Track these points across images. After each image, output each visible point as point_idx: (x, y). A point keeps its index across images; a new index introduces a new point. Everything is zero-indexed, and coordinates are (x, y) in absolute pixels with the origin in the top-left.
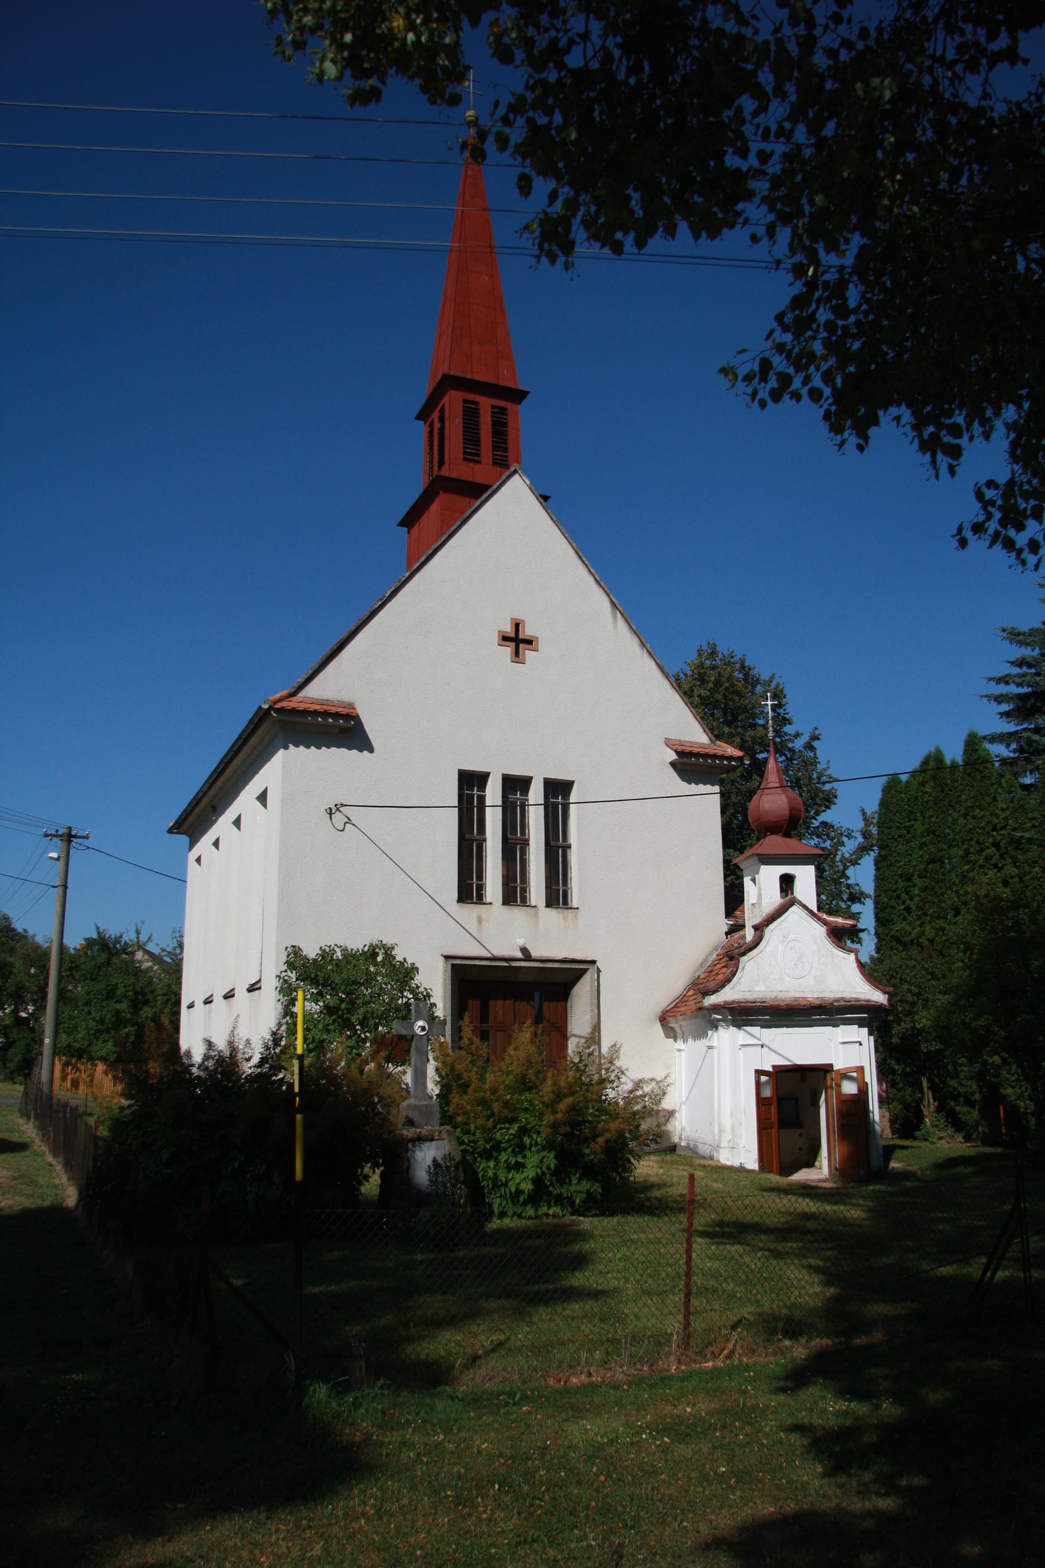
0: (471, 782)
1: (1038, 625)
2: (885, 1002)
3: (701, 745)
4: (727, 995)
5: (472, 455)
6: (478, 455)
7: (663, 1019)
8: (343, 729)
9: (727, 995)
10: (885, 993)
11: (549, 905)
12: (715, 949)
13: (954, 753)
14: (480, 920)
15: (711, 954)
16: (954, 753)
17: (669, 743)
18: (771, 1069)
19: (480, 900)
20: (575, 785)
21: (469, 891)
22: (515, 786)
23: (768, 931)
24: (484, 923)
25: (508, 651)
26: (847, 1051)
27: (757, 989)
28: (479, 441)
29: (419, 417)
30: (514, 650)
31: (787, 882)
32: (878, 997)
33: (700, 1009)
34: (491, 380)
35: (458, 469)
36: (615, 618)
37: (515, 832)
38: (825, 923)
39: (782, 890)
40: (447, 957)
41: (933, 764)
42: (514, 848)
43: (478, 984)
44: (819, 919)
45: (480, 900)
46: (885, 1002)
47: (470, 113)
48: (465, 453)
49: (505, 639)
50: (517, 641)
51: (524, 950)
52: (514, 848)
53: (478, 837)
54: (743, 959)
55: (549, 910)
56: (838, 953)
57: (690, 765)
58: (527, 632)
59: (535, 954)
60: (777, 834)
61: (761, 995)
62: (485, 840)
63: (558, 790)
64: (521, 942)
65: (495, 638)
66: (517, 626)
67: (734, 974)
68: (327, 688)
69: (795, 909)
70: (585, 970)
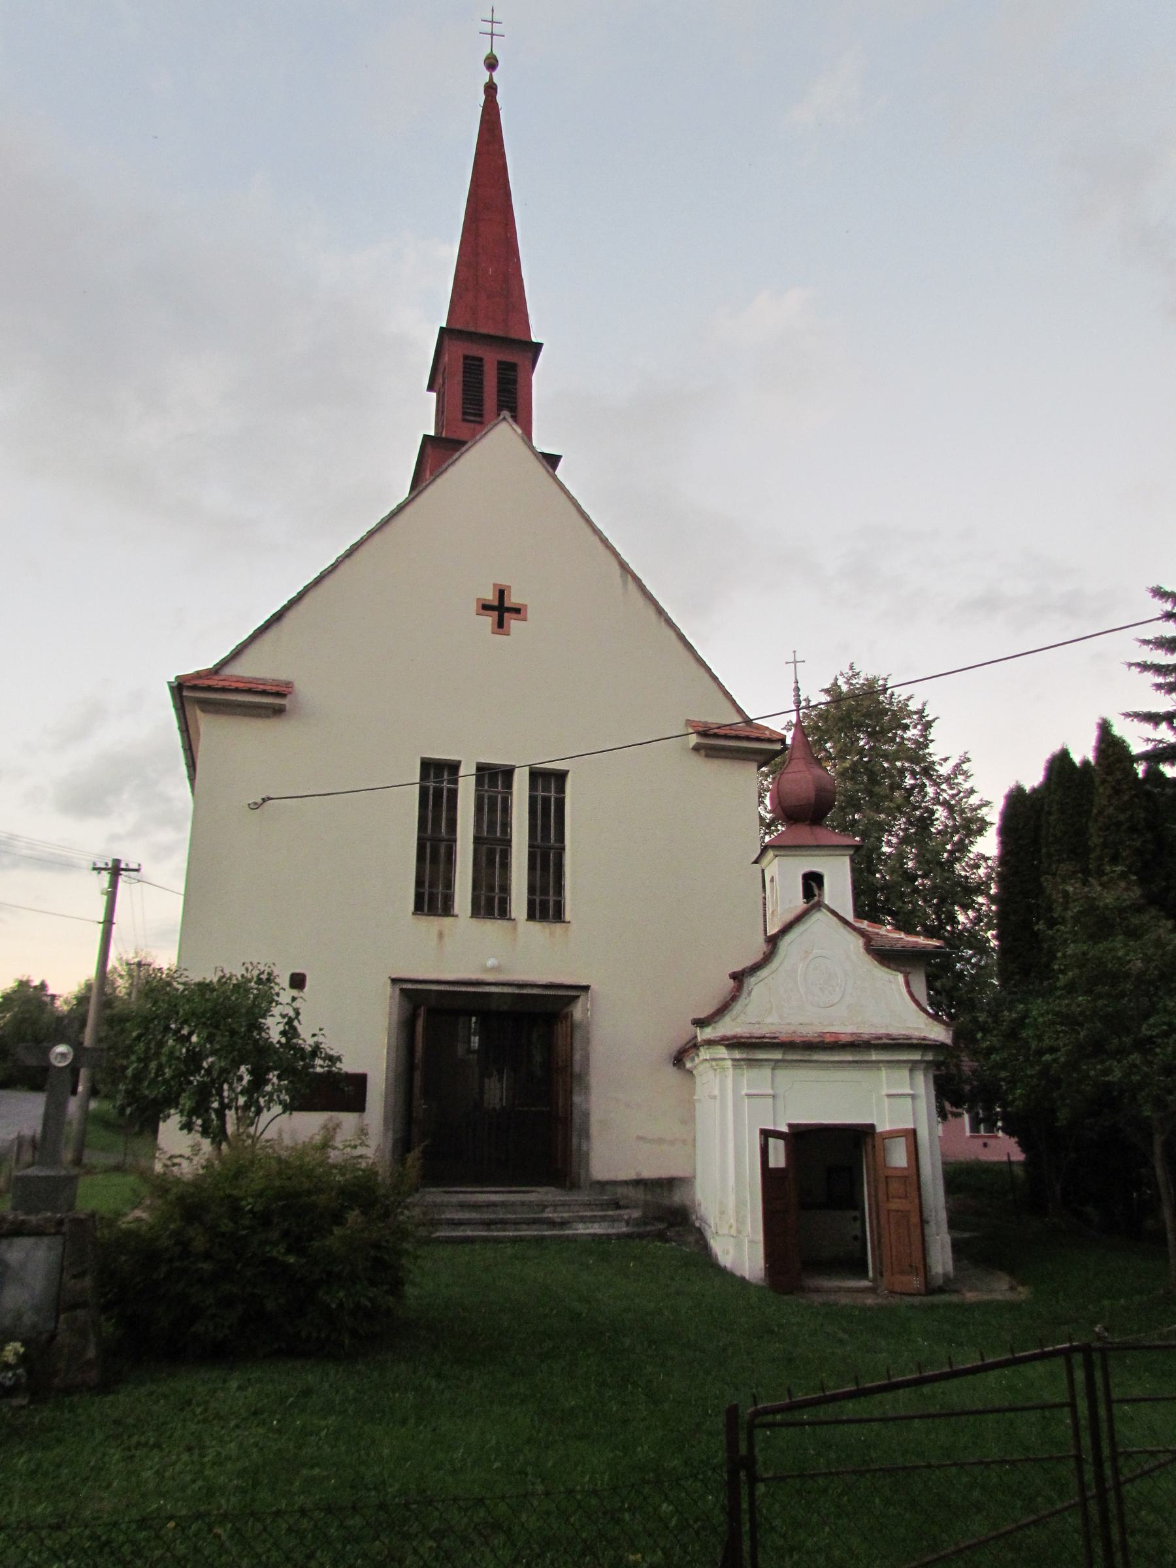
0: (437, 775)
1: (1171, 709)
2: (948, 1041)
6: (481, 415)
9: (727, 1027)
11: (531, 916)
13: (1083, 751)
14: (441, 935)
16: (1083, 751)
18: (785, 1129)
19: (447, 909)
20: (570, 775)
21: (432, 898)
22: (495, 778)
24: (446, 939)
26: (891, 1102)
27: (769, 1020)
28: (482, 400)
31: (812, 882)
32: (939, 1033)
34: (501, 333)
36: (625, 583)
38: (862, 933)
40: (394, 981)
41: (1060, 764)
43: (432, 1015)
44: (855, 929)
46: (948, 1041)
48: (464, 413)
49: (486, 607)
50: (501, 610)
53: (557, 845)
55: (531, 923)
58: (513, 599)
61: (773, 1029)
62: (455, 841)
65: (473, 606)
66: (501, 593)
70: (578, 997)
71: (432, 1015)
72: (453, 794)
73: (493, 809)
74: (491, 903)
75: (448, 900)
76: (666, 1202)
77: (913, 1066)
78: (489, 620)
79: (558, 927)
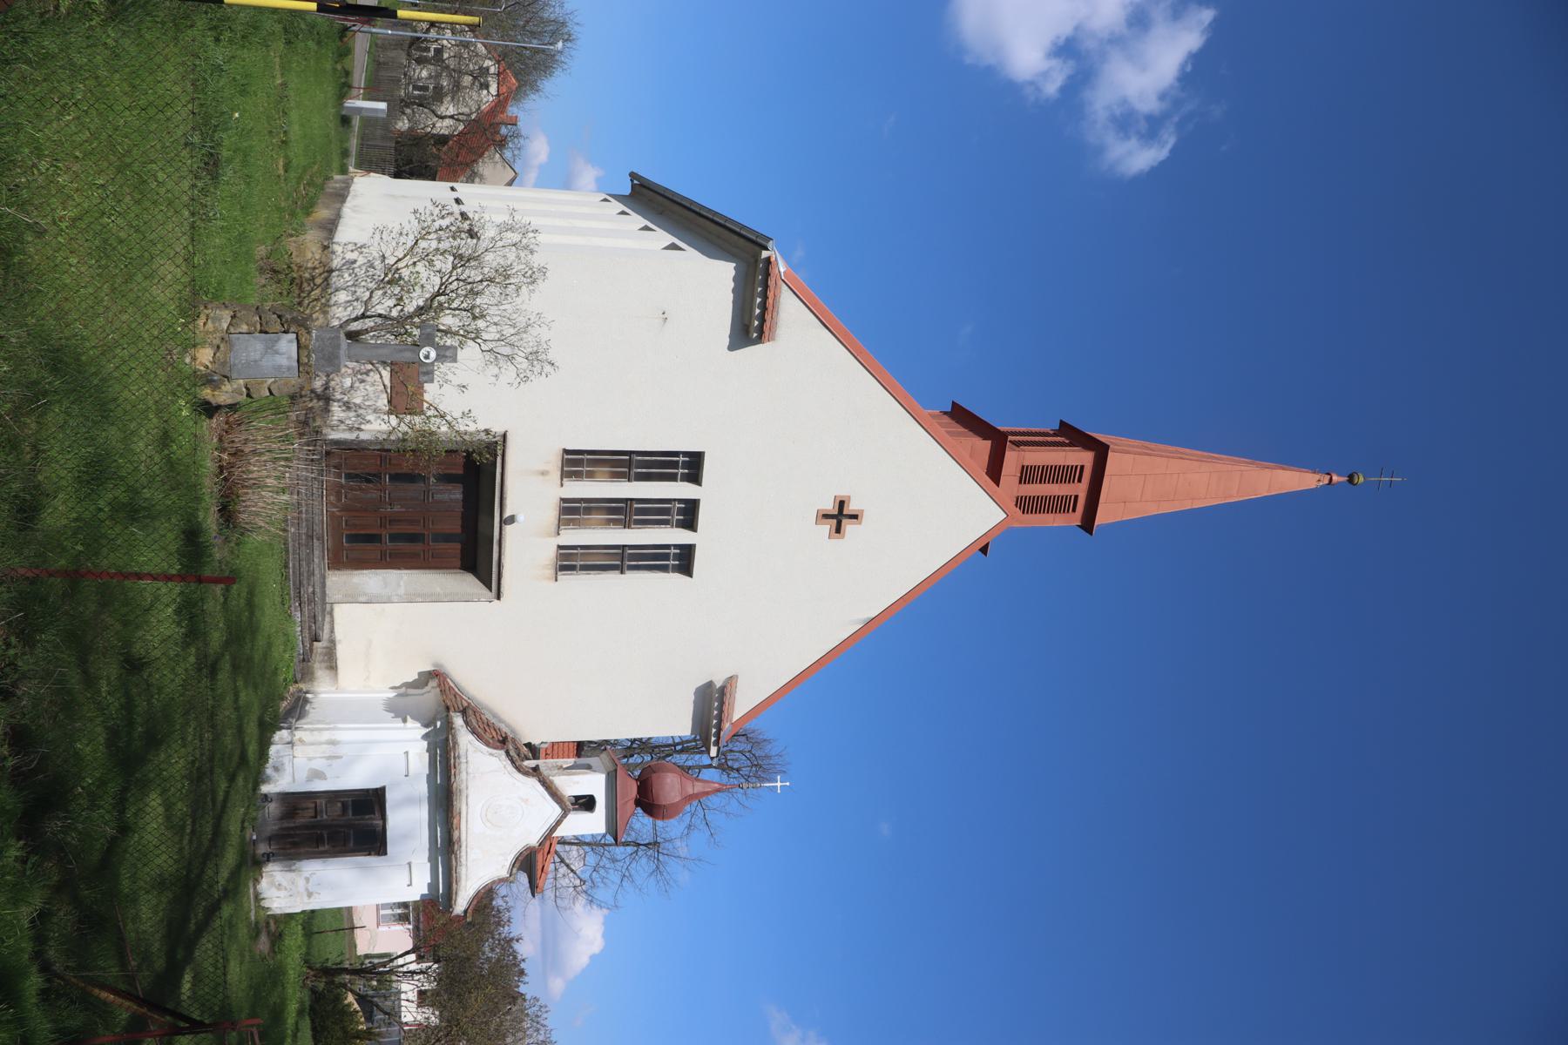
0: (693, 466)
3: (730, 715)
4: (466, 741)
5: (1028, 474)
7: (435, 676)
8: (750, 325)
10: (466, 912)
12: (513, 731)
14: (544, 473)
15: (508, 726)
17: (731, 680)
19: (565, 475)
21: (576, 463)
22: (688, 514)
23: (533, 782)
25: (830, 506)
29: (1062, 423)
30: (835, 503)
31: (587, 803)
32: (461, 904)
33: (448, 708)
35: (1013, 460)
37: (646, 506)
39: (577, 798)
40: (505, 436)
42: (623, 512)
43: (476, 470)
45: (565, 475)
47: (1362, 479)
50: (840, 516)
51: (512, 520)
52: (623, 512)
54: (502, 752)
56: (510, 858)
57: (711, 701)
59: (508, 529)
60: (639, 792)
63: (684, 560)
64: (520, 518)
65: (843, 493)
67: (487, 744)
68: (790, 311)
69: (558, 811)
70: (490, 589)
71: (476, 470)
72: (672, 478)
73: (654, 512)
74: (572, 511)
75: (577, 475)
76: (317, 665)
77: (433, 886)
78: (852, 507)
79: (551, 572)
